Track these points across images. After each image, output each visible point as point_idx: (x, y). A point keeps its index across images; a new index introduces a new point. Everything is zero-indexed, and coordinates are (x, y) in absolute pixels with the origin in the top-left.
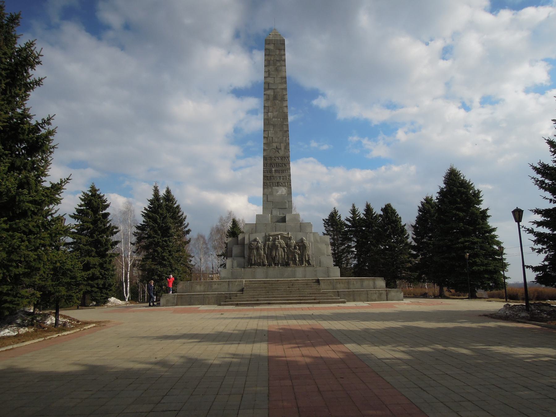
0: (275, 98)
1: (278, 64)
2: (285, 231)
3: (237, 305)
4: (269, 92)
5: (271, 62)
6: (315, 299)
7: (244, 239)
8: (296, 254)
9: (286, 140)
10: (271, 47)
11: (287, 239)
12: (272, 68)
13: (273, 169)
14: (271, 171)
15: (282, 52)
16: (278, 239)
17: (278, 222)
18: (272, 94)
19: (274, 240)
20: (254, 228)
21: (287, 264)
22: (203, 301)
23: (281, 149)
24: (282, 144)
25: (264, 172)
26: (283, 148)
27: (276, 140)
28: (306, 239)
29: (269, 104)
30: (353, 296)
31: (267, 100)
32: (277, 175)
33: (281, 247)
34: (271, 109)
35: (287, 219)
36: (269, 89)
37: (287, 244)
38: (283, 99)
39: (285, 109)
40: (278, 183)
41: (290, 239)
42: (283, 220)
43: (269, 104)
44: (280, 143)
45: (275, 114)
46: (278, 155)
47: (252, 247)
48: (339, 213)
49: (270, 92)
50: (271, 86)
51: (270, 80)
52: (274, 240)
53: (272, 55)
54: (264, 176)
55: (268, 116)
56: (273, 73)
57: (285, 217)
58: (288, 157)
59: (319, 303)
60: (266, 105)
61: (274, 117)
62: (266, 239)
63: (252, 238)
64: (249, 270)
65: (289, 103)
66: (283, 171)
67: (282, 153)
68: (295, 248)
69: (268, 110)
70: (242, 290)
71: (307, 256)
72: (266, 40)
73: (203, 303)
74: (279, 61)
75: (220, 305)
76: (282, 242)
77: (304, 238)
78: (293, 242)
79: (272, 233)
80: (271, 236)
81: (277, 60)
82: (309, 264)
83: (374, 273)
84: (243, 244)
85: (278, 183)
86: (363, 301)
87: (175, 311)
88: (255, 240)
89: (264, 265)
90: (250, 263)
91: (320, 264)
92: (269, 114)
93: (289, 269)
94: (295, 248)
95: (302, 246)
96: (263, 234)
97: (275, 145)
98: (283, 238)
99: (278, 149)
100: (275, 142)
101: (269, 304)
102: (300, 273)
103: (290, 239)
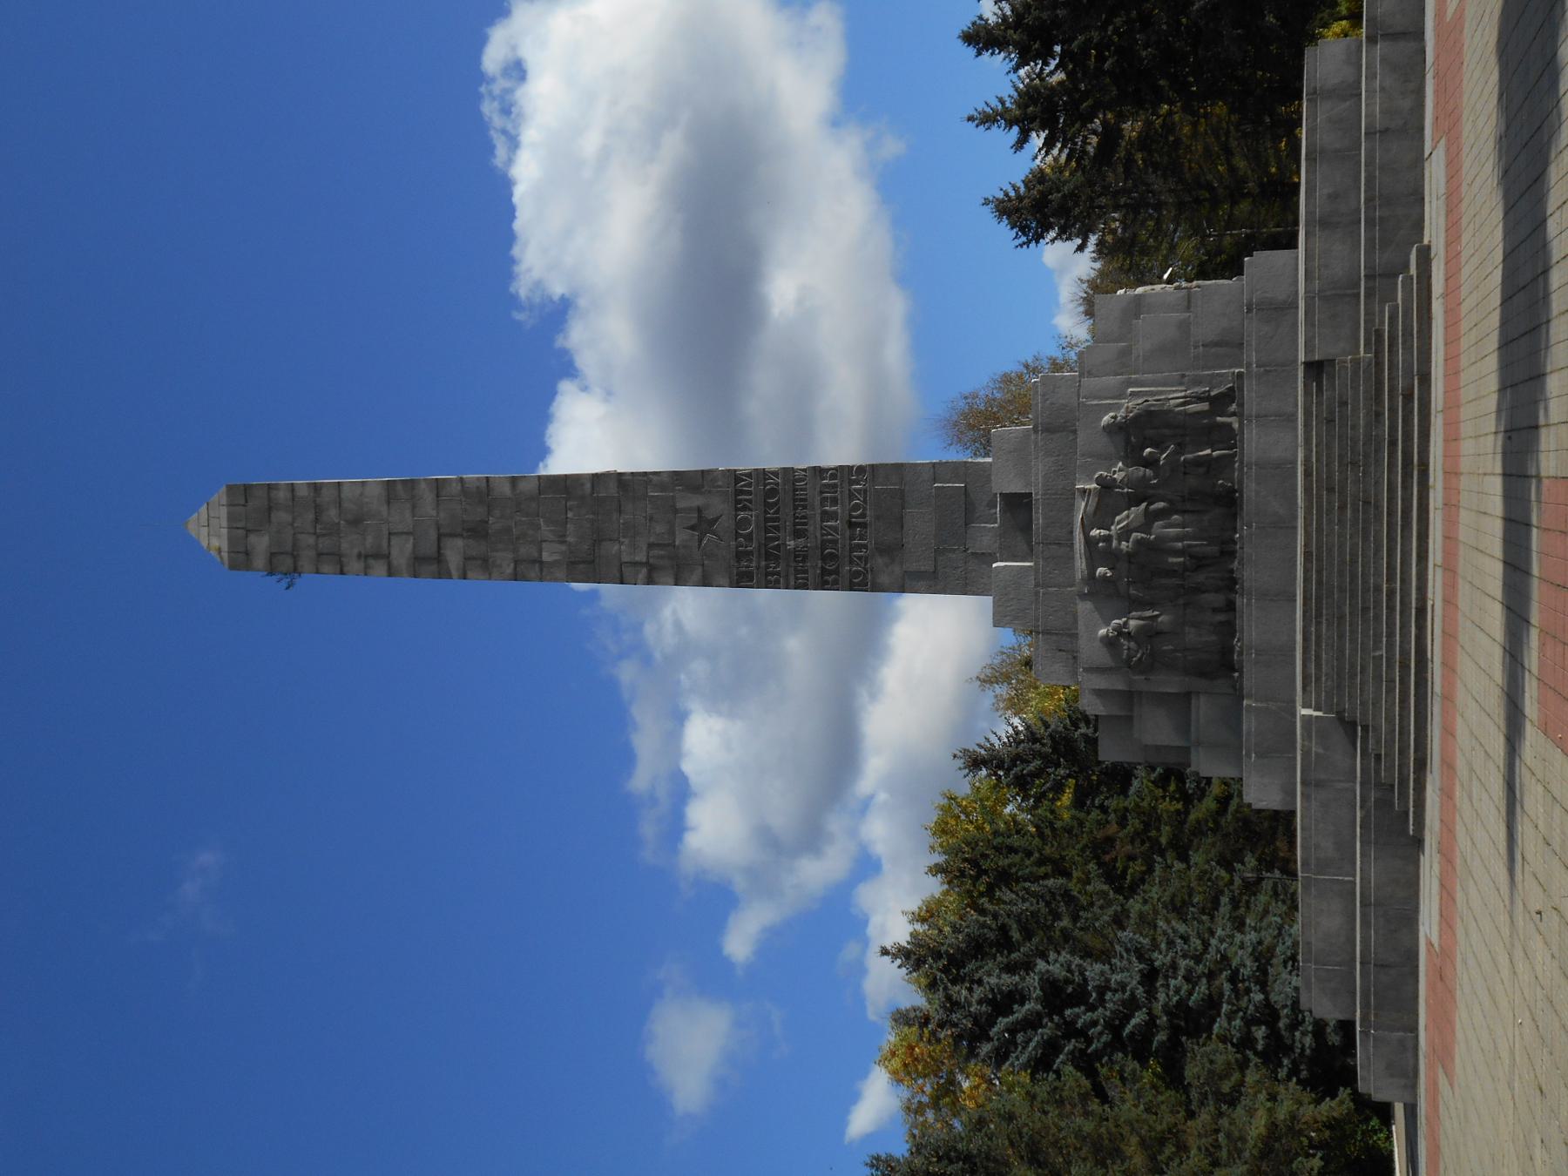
0: (477, 531)
1: (333, 513)
2: (1071, 508)
3: (1421, 765)
4: (453, 557)
5: (325, 544)
6: (1408, 397)
7: (1099, 693)
8: (1183, 463)
9: (662, 487)
10: (261, 544)
11: (1109, 499)
12: (350, 544)
13: (791, 544)
14: (800, 556)
15: (282, 495)
16: (1107, 539)
17: (1026, 528)
18: (459, 542)
19: (1111, 557)
20: (1058, 637)
21: (1230, 501)
22: (1400, 913)
23: (699, 510)
24: (680, 505)
25: (805, 587)
26: (697, 501)
27: (660, 528)
28: (1109, 408)
29: (504, 559)
30: (1399, 209)
31: (486, 566)
32: (814, 528)
33: (1146, 527)
34: (525, 550)
35: (1016, 487)
36: (439, 558)
37: (1134, 501)
38: (483, 494)
39: (523, 486)
40: (851, 525)
41: (1106, 486)
42: (1018, 504)
43: (504, 559)
44: (676, 511)
45: (546, 530)
46: (726, 523)
47: (1140, 656)
48: (972, 747)
49: (454, 552)
50: (429, 548)
51: (401, 551)
52: (1111, 557)
53: (295, 545)
54: (823, 585)
55: (555, 563)
56: (369, 540)
57: (1007, 498)
58: (735, 476)
59: (1425, 379)
60: (509, 570)
61: (562, 539)
62: (1098, 590)
63: (1103, 657)
64: (1251, 677)
65: (499, 474)
66: (800, 502)
67: (718, 506)
68: (1150, 463)
69: (534, 562)
70: (1349, 726)
71: (1192, 407)
72: (233, 566)
73: (1408, 917)
74: (319, 510)
75: (1418, 842)
76: (1122, 520)
77: (1106, 419)
78: (1119, 472)
79: (1080, 564)
80: (1092, 568)
81: (317, 520)
82: (1229, 396)
83: (1272, 96)
84: (1129, 698)
85: (851, 525)
86: (1418, 162)
87: (1444, 1055)
88: (1110, 643)
89: (1231, 607)
90: (1221, 664)
91: (1230, 345)
92: (546, 557)
93: (1251, 491)
94: (1150, 463)
95: (1138, 433)
96: (1084, 608)
97: (681, 537)
98: (1102, 515)
99: (702, 524)
100: (672, 533)
101: (1422, 611)
102: (1278, 442)
103: (1106, 486)
